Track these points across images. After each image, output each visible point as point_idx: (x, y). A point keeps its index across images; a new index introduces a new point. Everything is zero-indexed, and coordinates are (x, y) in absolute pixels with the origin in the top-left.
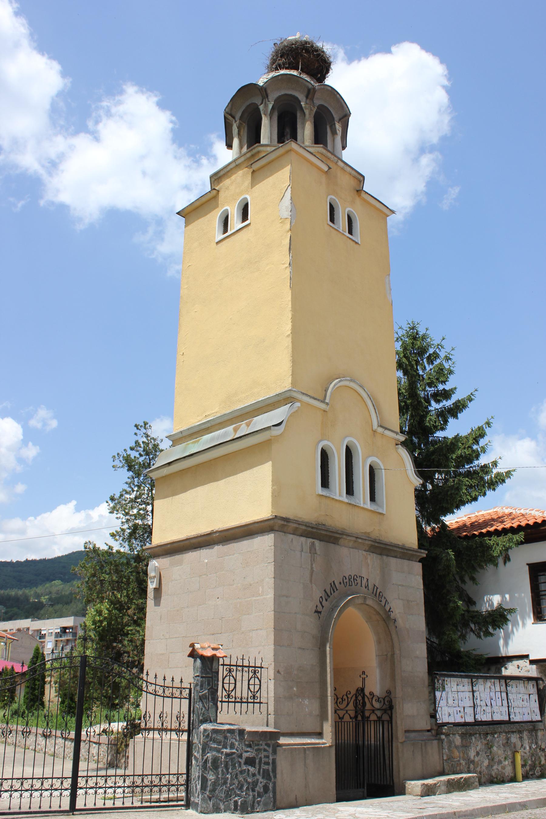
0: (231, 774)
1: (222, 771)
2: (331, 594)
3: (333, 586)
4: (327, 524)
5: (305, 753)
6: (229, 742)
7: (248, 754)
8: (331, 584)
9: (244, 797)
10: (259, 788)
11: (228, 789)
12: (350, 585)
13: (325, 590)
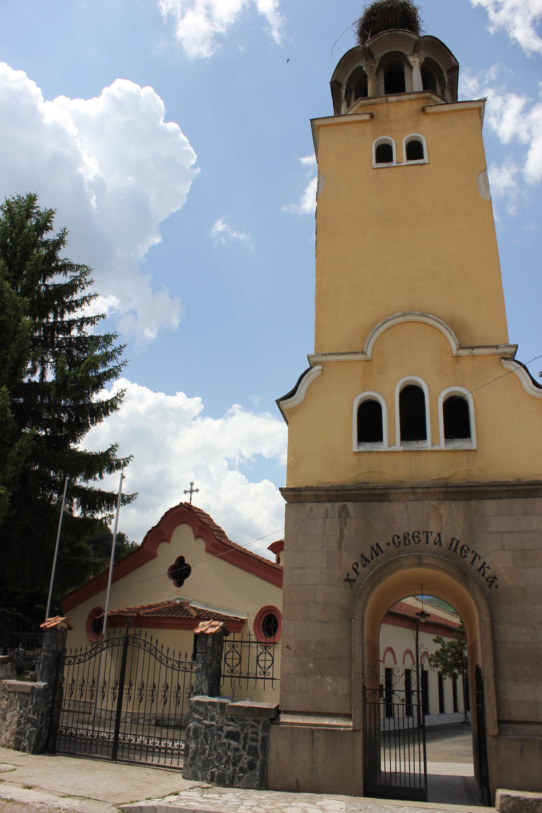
0: (210, 745)
1: (202, 741)
2: (372, 558)
3: (376, 550)
4: (371, 481)
5: (313, 735)
6: (210, 715)
7: (230, 728)
8: (372, 547)
9: (222, 770)
10: (243, 763)
11: (206, 759)
12: (405, 544)
13: (362, 556)
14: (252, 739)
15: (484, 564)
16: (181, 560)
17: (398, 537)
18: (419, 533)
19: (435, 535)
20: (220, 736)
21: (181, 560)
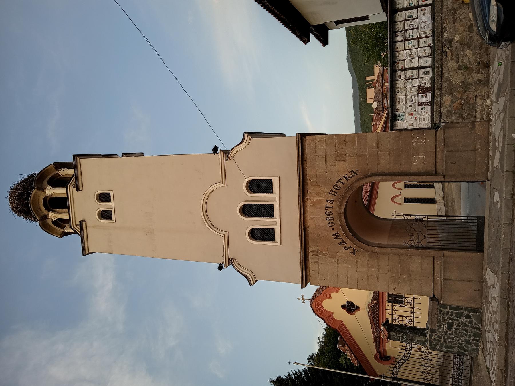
2: (341, 239)
8: (335, 238)
14: (452, 315)
15: (344, 177)
16: (343, 307)
17: (329, 223)
18: (326, 212)
19: (327, 203)
20: (450, 334)
21: (343, 307)
